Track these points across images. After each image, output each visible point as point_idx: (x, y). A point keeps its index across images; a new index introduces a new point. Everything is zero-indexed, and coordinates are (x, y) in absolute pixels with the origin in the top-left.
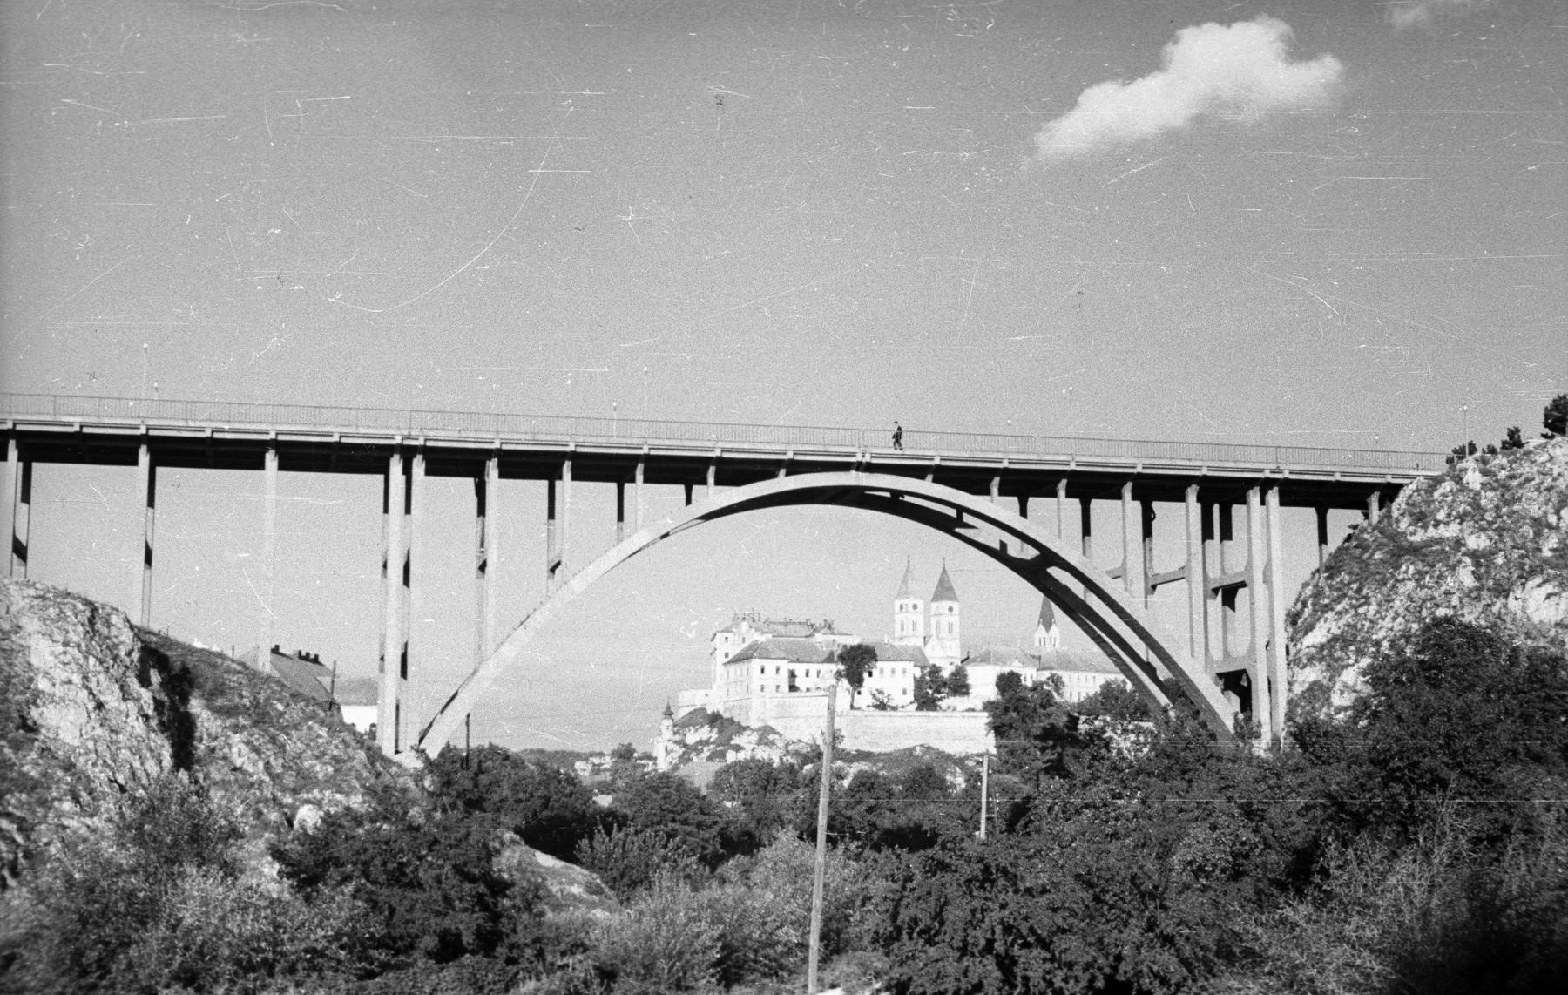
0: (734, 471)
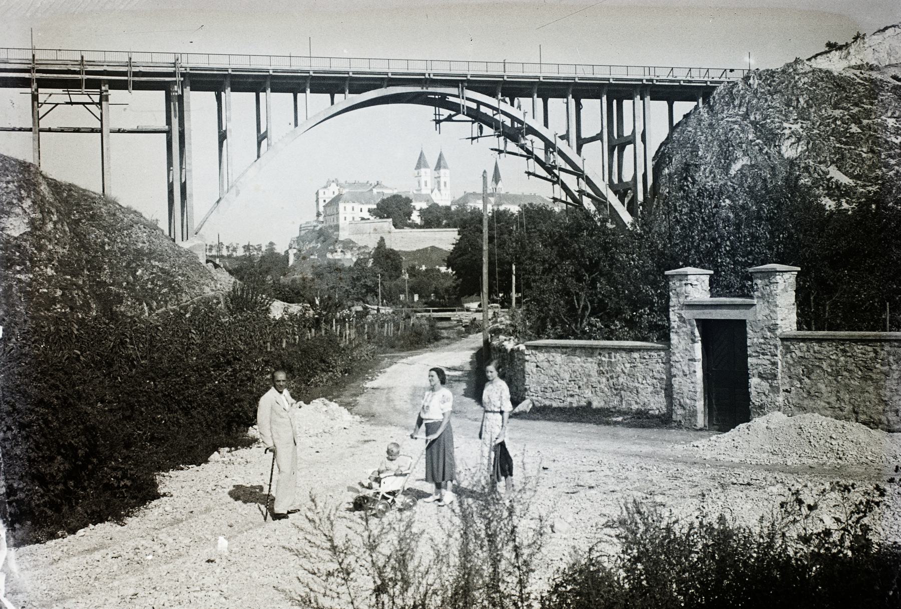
0: (358, 84)
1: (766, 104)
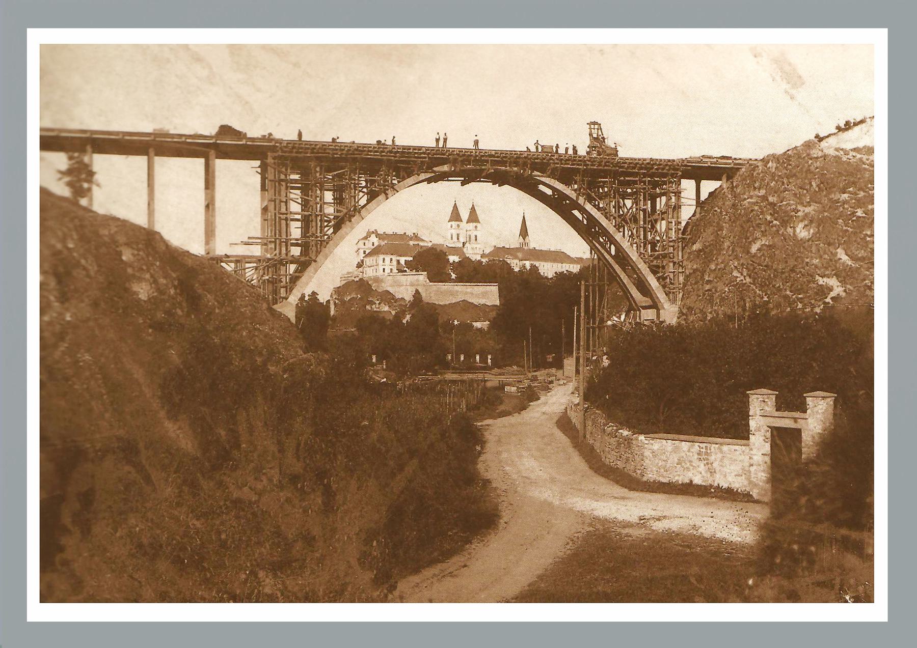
1: (783, 187)
